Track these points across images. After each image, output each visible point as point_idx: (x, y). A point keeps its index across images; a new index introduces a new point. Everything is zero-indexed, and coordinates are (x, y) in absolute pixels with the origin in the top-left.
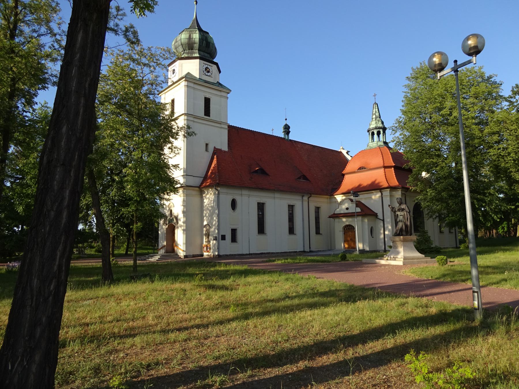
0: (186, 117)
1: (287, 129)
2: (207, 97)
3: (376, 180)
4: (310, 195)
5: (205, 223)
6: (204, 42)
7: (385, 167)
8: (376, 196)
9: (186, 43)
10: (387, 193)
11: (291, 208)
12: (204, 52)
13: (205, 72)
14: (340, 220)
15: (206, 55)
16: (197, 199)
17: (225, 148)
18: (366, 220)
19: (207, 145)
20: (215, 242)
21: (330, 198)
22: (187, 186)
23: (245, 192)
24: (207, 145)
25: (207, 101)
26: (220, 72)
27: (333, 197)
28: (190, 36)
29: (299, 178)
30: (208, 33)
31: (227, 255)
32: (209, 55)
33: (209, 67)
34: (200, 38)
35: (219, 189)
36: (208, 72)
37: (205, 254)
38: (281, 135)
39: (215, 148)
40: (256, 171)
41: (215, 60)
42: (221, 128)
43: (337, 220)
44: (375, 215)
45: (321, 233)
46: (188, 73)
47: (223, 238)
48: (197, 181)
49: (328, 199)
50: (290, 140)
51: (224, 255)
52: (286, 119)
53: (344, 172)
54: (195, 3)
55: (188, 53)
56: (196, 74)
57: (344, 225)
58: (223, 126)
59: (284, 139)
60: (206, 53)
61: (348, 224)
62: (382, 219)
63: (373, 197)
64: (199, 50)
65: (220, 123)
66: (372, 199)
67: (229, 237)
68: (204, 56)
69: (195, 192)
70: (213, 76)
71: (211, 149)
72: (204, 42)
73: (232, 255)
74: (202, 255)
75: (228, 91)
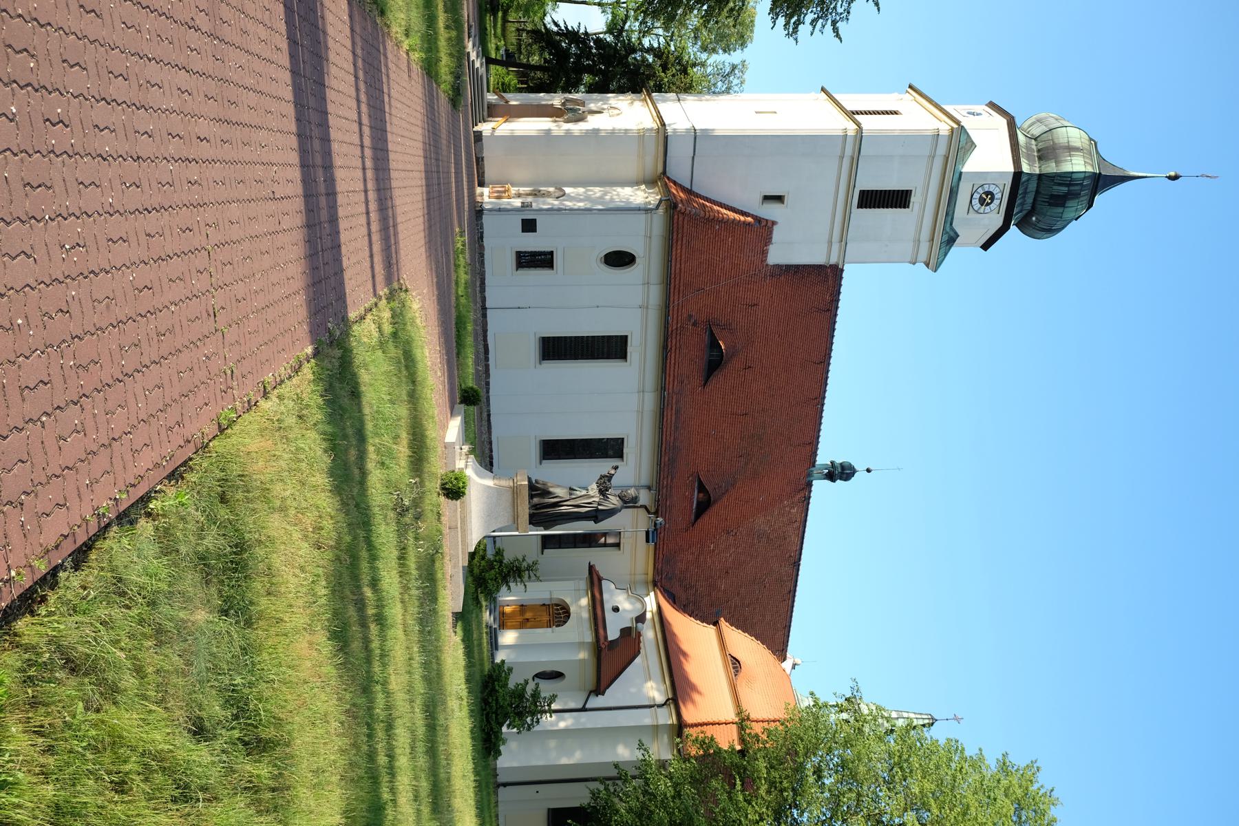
0: (851, 133)
1: (842, 472)
2: (913, 199)
3: (699, 692)
4: (653, 510)
5: (568, 190)
6: (1065, 189)
7: (679, 100)
8: (655, 691)
9: (1056, 141)
10: (666, 718)
11: (611, 448)
12: (1037, 192)
13: (981, 191)
14: (582, 592)
15: (1030, 200)
16: (632, 169)
17: (777, 255)
18: (583, 655)
19: (779, 199)
20: (520, 205)
21: (647, 583)
22: (666, 138)
23: (655, 295)
24: (779, 199)
25: (899, 199)
26: (986, 246)
27: (651, 587)
28: (1077, 149)
29: (702, 488)
30: (1090, 205)
31: (481, 238)
32: (1028, 207)
33: (996, 202)
34: (1074, 176)
35: (661, 211)
36: (982, 201)
37: (486, 191)
38: (824, 457)
39: (774, 223)
40: (714, 344)
41: (1013, 229)
42: (830, 243)
43: (583, 584)
44: (599, 690)
45: (546, 551)
46: (972, 145)
47: (529, 226)
48: (680, 171)
49: (643, 577)
50: (810, 485)
51: (482, 227)
52: (868, 471)
53: (723, 623)
54: (1173, 174)
55: (1028, 148)
56: (972, 165)
57: (568, 601)
58: (835, 247)
59: (813, 463)
60: (1035, 200)
61: (572, 609)
62: (588, 706)
63: (650, 684)
64: (1040, 176)
65: (843, 240)
66: (646, 681)
67: (532, 243)
68: (1025, 193)
69: (651, 164)
70: (972, 215)
71: (770, 212)
72: (1065, 189)
73: (482, 255)
74: (481, 184)
75: (934, 264)
